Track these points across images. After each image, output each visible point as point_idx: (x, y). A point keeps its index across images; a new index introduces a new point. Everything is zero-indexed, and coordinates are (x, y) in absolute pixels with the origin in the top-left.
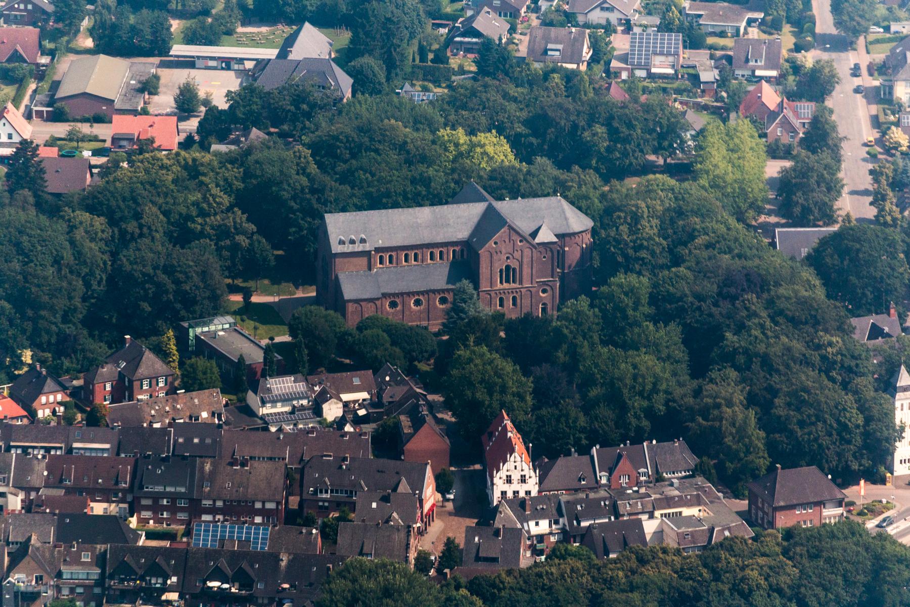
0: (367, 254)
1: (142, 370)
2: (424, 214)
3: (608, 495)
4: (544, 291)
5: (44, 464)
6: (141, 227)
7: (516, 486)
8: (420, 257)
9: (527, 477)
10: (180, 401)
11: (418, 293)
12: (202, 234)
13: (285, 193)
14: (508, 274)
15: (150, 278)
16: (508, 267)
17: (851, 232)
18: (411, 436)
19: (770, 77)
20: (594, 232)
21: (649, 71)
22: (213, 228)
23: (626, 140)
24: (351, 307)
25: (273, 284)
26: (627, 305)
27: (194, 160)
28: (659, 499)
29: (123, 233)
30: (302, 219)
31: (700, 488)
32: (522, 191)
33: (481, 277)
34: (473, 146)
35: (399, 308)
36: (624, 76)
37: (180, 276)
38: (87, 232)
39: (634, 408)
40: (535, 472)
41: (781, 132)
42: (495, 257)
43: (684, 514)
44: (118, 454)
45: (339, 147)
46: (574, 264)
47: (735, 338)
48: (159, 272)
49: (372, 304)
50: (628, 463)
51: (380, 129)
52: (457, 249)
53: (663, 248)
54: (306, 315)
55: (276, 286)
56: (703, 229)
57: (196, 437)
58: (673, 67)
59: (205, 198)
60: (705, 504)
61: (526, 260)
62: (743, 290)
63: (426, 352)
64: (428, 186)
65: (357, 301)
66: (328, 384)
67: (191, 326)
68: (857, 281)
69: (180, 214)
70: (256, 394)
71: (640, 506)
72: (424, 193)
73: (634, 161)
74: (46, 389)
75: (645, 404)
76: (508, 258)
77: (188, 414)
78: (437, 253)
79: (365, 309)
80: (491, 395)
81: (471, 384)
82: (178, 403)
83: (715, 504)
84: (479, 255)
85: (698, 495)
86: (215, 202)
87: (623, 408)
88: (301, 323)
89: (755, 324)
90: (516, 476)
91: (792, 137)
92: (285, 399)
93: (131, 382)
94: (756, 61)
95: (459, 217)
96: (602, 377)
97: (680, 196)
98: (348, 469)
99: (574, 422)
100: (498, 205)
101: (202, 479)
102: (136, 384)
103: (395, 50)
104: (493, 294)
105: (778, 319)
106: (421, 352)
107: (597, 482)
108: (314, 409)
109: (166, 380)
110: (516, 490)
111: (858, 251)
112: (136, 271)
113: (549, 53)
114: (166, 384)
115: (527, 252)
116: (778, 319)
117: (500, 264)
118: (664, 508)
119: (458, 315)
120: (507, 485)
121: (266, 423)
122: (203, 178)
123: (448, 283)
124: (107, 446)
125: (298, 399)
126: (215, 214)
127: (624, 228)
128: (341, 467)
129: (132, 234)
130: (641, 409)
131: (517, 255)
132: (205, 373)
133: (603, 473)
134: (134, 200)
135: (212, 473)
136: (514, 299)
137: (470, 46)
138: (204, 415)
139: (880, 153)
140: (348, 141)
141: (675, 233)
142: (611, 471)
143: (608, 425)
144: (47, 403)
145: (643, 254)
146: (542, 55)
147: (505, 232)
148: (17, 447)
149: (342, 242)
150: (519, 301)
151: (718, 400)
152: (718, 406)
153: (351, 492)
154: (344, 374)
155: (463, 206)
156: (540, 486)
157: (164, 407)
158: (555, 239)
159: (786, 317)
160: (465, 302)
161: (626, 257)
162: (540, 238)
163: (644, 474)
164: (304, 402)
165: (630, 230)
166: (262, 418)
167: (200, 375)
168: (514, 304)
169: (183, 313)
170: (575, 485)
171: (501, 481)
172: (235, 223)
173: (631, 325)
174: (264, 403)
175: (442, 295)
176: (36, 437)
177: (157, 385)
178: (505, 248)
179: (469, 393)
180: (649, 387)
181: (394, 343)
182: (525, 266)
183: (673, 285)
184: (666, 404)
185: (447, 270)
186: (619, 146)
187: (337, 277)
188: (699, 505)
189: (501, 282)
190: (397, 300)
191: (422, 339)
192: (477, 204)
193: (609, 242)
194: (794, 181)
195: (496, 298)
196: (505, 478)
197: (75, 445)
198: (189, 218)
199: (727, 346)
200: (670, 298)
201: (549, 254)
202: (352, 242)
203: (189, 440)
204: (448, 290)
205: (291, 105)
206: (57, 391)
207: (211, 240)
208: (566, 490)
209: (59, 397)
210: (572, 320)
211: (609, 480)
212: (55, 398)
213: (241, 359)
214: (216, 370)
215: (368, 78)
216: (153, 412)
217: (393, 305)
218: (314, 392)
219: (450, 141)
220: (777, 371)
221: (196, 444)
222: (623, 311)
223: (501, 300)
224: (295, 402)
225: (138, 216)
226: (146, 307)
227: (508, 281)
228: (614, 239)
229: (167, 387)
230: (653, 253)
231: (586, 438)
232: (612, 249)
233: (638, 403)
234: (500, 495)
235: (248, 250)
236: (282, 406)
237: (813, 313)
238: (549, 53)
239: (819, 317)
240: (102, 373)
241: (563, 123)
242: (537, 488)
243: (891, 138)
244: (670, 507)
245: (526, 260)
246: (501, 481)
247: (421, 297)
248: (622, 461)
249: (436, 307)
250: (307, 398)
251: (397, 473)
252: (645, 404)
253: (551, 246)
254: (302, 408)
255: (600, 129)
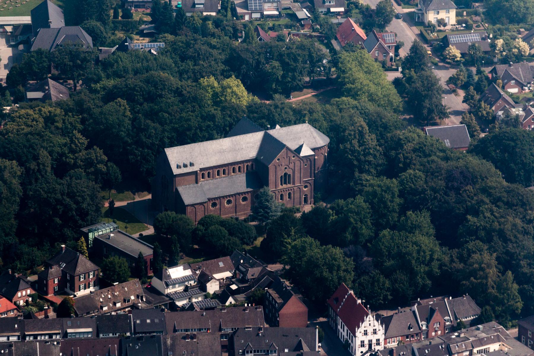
0: (195, 173)
1: (79, 269)
2: (225, 143)
3: (443, 341)
4: (306, 187)
5: (59, 348)
6: (38, 165)
7: (370, 337)
8: (227, 171)
9: (377, 330)
10: (116, 290)
11: (229, 196)
12: (75, 166)
14: (286, 179)
15: (58, 202)
16: (285, 174)
17: (507, 135)
18: (282, 306)
19: (339, 12)
20: (330, 146)
21: (262, 14)
22: (82, 161)
23: (294, 70)
24: (189, 209)
25: (119, 193)
26: (387, 199)
27: (50, 112)
28: (475, 340)
29: (28, 170)
30: (136, 149)
31: (497, 330)
33: (269, 182)
34: (224, 88)
35: (218, 206)
36: (247, 18)
37: (79, 198)
38: (10, 173)
39: (420, 272)
40: (382, 326)
41: (378, 54)
42: (278, 169)
43: (491, 350)
44: (98, 336)
45: (137, 95)
46: (320, 167)
47: (475, 219)
48: (65, 197)
49: (202, 206)
50: (439, 314)
51: (160, 81)
52: (249, 164)
53: (381, 153)
55: (121, 194)
56: (406, 138)
57: (148, 318)
58: (277, 10)
59: (72, 141)
60: (503, 341)
61: (297, 169)
62: (461, 183)
63: (252, 238)
64: (214, 122)
65: (193, 205)
66: (204, 269)
67: (90, 231)
68: (515, 167)
69: (58, 153)
70: (161, 280)
71: (464, 347)
73: (299, 83)
74: (20, 287)
75: (427, 269)
76: (286, 168)
77: (123, 298)
80: (331, 272)
81: (317, 266)
82: (115, 292)
83: (509, 340)
84: (268, 168)
85: (498, 335)
86: (79, 142)
87: (412, 273)
89: (486, 209)
90: (370, 330)
91: (385, 56)
92: (181, 281)
93: (72, 278)
94: (330, 2)
95: (248, 143)
96: (387, 251)
97: (363, 112)
98: (263, 336)
99: (383, 285)
100: (271, 132)
101: (166, 350)
102: (76, 278)
103: (104, 13)
104: (277, 192)
105: (498, 203)
107: (420, 329)
108: (199, 287)
109: (94, 273)
110: (370, 339)
111: (514, 148)
112: (51, 198)
113: (197, 6)
114: (94, 276)
115: (298, 163)
116: (498, 203)
117: (281, 173)
118: (479, 346)
120: (365, 337)
121: (171, 299)
122: (57, 124)
124: (90, 330)
125: (188, 281)
126: (80, 151)
127: (355, 142)
128: (258, 335)
129: (34, 170)
130: (425, 272)
131: (292, 166)
132: (120, 267)
133: (423, 322)
134: (31, 146)
135: (173, 345)
136: (290, 194)
137: (137, 4)
138: (133, 298)
139: (439, 62)
140: (141, 90)
141: (386, 142)
142: (428, 320)
143: (404, 285)
144: (22, 296)
145: (371, 158)
146: (191, 8)
147: (284, 152)
148: (30, 335)
149: (178, 167)
150: (292, 195)
151: (483, 265)
152: (482, 269)
153: (268, 351)
155: (250, 135)
156: (385, 335)
157: (107, 295)
158: (313, 153)
159: (503, 201)
160: (268, 202)
161: (359, 160)
162: (303, 153)
163: (448, 321)
164: (192, 283)
165: (359, 142)
166: (167, 296)
167: (118, 269)
168: (290, 197)
169: (80, 222)
170: (407, 332)
171: (361, 334)
172: (96, 156)
173: (390, 212)
174: (167, 285)
175: (244, 196)
176: (42, 327)
177: (89, 277)
178: (284, 162)
180: (428, 258)
181: (231, 234)
182: (296, 172)
183: (413, 183)
184: (440, 267)
185: (245, 178)
186: (290, 74)
188: (499, 341)
189: (281, 184)
190: (216, 202)
191: (249, 230)
192: (257, 133)
194: (423, 93)
195: (279, 195)
196: (363, 332)
197: (69, 331)
198: (62, 155)
199: (471, 225)
200: (414, 192)
201: (309, 162)
202: (185, 166)
203: (143, 321)
204: (247, 192)
205: (70, 61)
206: (28, 288)
207: (82, 169)
208: (401, 336)
209: (29, 292)
210: (355, 212)
211: (427, 327)
212: (26, 292)
213: (140, 254)
214: (127, 264)
215: (98, 35)
216: (101, 300)
217: (214, 205)
220: (510, 240)
221: (149, 323)
222: (385, 203)
223: (282, 196)
224: (186, 283)
225: (36, 158)
226: (58, 220)
227: (285, 183)
228: (350, 150)
229: (95, 278)
230: (375, 156)
231: (391, 295)
232: (350, 156)
233: (423, 269)
234: (360, 343)
235: (107, 174)
236: (179, 287)
237: (520, 198)
238: (197, 6)
239: (524, 201)
240: (51, 272)
241: (251, 60)
242: (383, 336)
243: (450, 53)
244: (482, 345)
245: (297, 169)
246: (361, 334)
247: (231, 199)
248: (435, 314)
249: (240, 204)
250: (194, 279)
251: (297, 336)
252: (427, 269)
253: (310, 158)
254: (192, 287)
255: (276, 64)
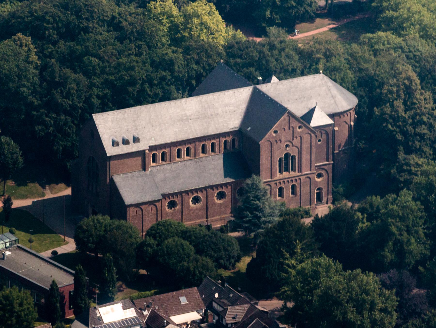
0: (142, 154)
4: (319, 176)
8: (192, 151)
11: (196, 190)
13: (25, 89)
16: (287, 155)
20: (358, 110)
24: (132, 212)
25: (19, 185)
30: (47, 116)
32: (273, 68)
34: (188, 17)
35: (178, 207)
42: (275, 147)
45: (48, 29)
46: (343, 144)
49: (152, 206)
51: (86, 5)
52: (229, 139)
54: (96, 228)
55: (22, 188)
61: (305, 146)
65: (138, 205)
66: (157, 307)
72: (169, 77)
73: (309, 9)
76: (287, 146)
78: (208, 144)
79: (145, 213)
80: (360, 312)
81: (337, 303)
88: (91, 235)
95: (226, 106)
100: (264, 88)
104: (273, 184)
106: (229, 260)
119: (252, 213)
123: (226, 176)
127: (399, 104)
131: (297, 142)
132: (21, 305)
136: (293, 187)
140: (55, 20)
145: (424, 130)
147: (284, 119)
149: (115, 143)
150: (298, 189)
154: (170, 294)
155: (230, 92)
160: (259, 199)
165: (405, 103)
167: (17, 308)
168: (293, 192)
175: (220, 190)
178: (285, 136)
179: (337, 313)
181: (199, 251)
182: (304, 153)
185: (221, 162)
187: (112, 180)
189: (280, 172)
190: (176, 199)
191: (228, 246)
193: (385, 120)
195: (276, 188)
201: (324, 136)
202: (125, 142)
204: (226, 185)
214: (31, 300)
217: (172, 204)
218: (144, 316)
219: (163, 14)
227: (287, 170)
228: (391, 116)
232: (390, 126)
245: (305, 146)
247: (200, 195)
249: (214, 204)
253: (326, 129)
